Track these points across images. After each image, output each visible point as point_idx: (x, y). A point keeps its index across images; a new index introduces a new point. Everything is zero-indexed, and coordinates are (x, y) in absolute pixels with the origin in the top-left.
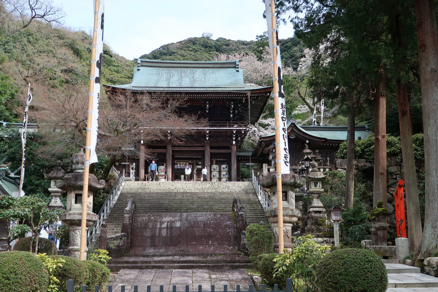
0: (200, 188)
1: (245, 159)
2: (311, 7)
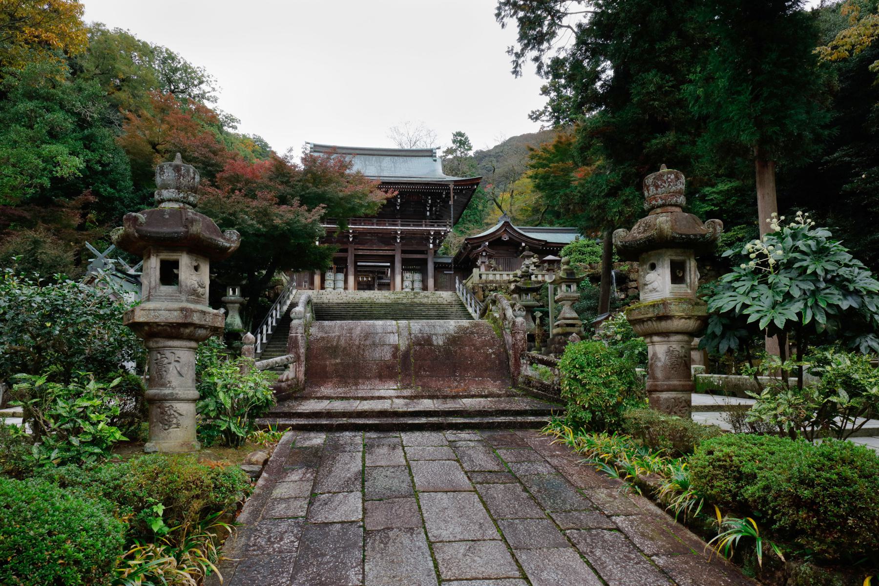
0: (358, 297)
2: (487, 293)
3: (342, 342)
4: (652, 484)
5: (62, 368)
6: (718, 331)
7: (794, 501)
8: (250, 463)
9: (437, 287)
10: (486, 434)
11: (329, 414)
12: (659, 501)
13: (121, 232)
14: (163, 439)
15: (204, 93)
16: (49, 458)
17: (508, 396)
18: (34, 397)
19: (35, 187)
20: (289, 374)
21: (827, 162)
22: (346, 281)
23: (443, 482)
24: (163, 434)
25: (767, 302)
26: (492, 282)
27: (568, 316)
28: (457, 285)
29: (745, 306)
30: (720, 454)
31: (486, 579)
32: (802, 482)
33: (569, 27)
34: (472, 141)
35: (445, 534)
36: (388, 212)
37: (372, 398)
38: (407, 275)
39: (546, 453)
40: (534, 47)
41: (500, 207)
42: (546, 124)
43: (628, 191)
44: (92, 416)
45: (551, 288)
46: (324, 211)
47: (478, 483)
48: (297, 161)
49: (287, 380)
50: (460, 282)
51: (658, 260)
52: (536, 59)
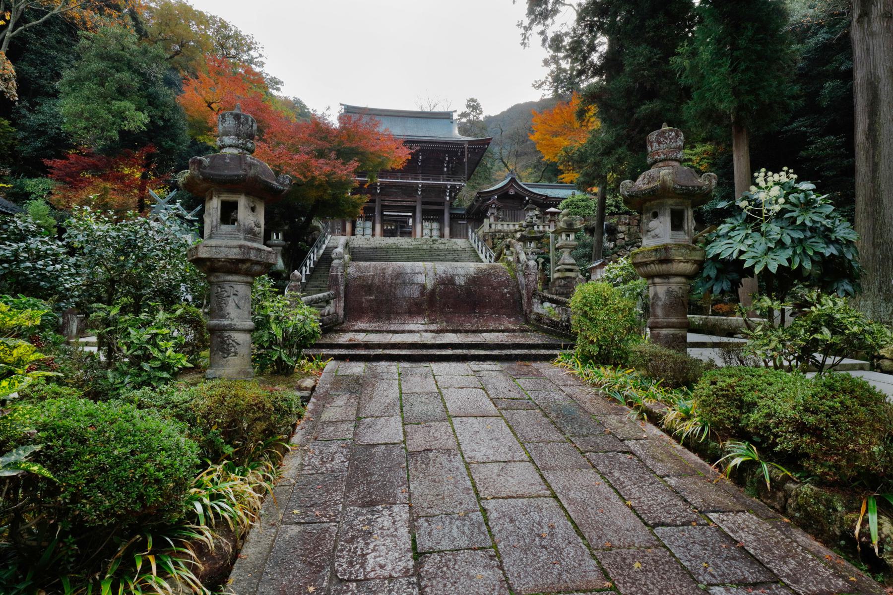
1: (460, 217)
2: (496, 241)
3: (376, 281)
4: (657, 411)
5: (132, 300)
6: (713, 273)
7: (798, 428)
8: (299, 388)
9: (452, 235)
10: (505, 365)
11: (367, 346)
12: (664, 427)
13: (187, 175)
14: (223, 366)
15: (253, 58)
16: (122, 382)
17: (522, 331)
18: (108, 326)
19: (106, 139)
20: (330, 309)
21: (787, 131)
22: (373, 229)
23: (472, 409)
24: (222, 362)
25: (760, 248)
26: (500, 231)
27: (567, 261)
28: (470, 234)
29: (741, 252)
30: (724, 385)
31: (520, 497)
32: (806, 410)
33: (571, 5)
34: (483, 107)
35: (480, 457)
36: (411, 168)
37: (403, 332)
38: (426, 224)
39: (560, 383)
40: (540, 22)
41: (506, 166)
42: (547, 92)
43: (620, 151)
44: (161, 343)
45: (552, 236)
46: (357, 164)
47: (503, 409)
48: (334, 121)
49: (329, 314)
50: (473, 231)
51: (660, 209)
52: (542, 33)
